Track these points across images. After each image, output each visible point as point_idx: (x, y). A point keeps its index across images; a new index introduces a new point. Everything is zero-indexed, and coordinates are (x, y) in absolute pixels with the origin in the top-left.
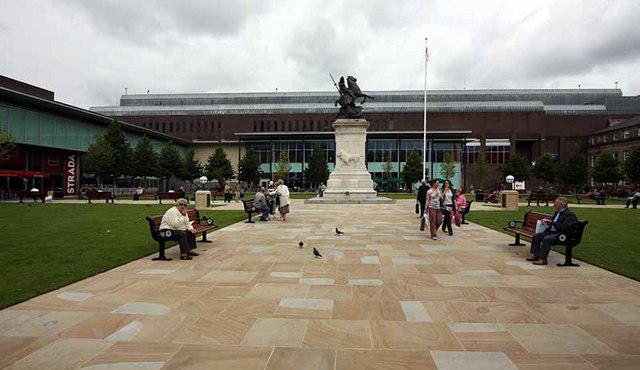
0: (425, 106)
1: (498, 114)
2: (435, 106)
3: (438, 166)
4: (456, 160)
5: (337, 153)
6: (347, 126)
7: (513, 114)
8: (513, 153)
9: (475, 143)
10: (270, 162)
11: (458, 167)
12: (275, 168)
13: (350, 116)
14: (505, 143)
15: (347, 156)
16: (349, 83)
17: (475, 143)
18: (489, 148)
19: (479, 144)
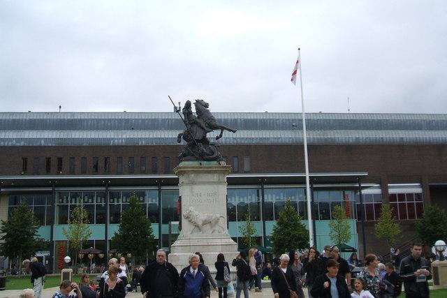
0: (305, 136)
1: (401, 148)
2: (318, 135)
3: (324, 226)
4: (348, 215)
5: (184, 213)
6: (197, 172)
7: (420, 148)
8: (428, 207)
9: (372, 190)
10: (51, 223)
11: (352, 224)
12: (62, 233)
13: (202, 157)
14: (414, 189)
15: (201, 216)
16: (197, 109)
17: (372, 190)
18: (393, 197)
19: (378, 191)
